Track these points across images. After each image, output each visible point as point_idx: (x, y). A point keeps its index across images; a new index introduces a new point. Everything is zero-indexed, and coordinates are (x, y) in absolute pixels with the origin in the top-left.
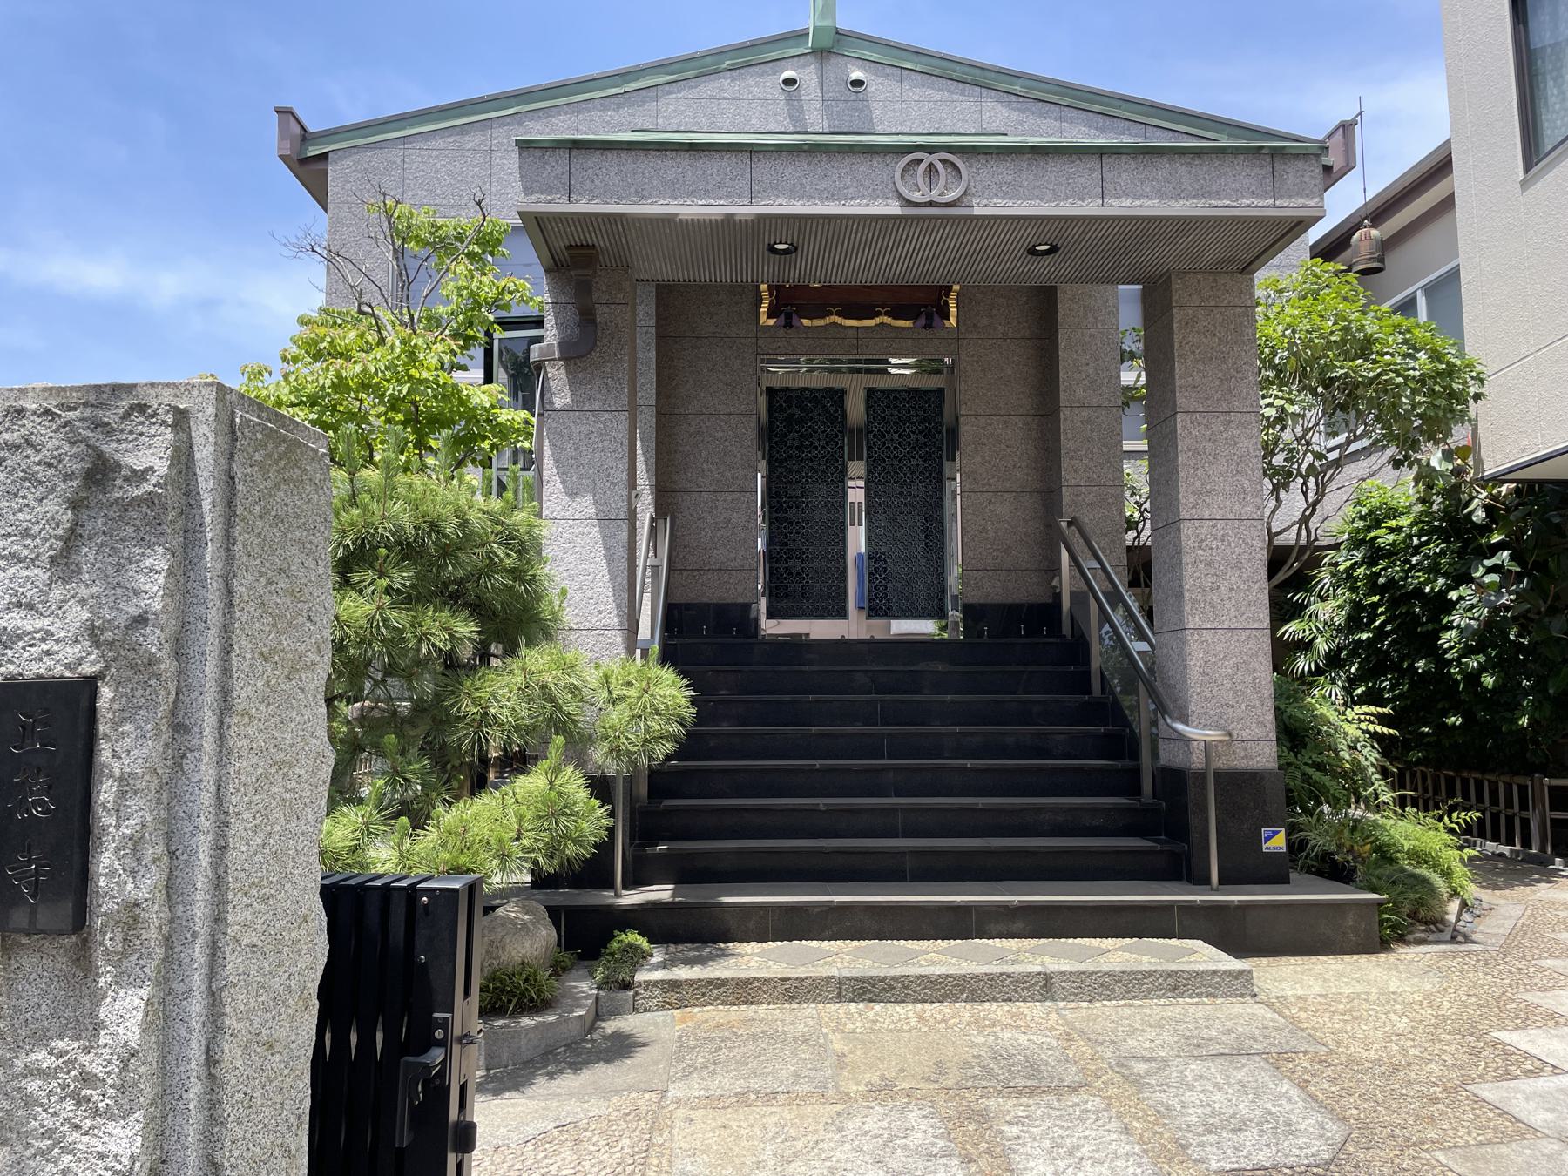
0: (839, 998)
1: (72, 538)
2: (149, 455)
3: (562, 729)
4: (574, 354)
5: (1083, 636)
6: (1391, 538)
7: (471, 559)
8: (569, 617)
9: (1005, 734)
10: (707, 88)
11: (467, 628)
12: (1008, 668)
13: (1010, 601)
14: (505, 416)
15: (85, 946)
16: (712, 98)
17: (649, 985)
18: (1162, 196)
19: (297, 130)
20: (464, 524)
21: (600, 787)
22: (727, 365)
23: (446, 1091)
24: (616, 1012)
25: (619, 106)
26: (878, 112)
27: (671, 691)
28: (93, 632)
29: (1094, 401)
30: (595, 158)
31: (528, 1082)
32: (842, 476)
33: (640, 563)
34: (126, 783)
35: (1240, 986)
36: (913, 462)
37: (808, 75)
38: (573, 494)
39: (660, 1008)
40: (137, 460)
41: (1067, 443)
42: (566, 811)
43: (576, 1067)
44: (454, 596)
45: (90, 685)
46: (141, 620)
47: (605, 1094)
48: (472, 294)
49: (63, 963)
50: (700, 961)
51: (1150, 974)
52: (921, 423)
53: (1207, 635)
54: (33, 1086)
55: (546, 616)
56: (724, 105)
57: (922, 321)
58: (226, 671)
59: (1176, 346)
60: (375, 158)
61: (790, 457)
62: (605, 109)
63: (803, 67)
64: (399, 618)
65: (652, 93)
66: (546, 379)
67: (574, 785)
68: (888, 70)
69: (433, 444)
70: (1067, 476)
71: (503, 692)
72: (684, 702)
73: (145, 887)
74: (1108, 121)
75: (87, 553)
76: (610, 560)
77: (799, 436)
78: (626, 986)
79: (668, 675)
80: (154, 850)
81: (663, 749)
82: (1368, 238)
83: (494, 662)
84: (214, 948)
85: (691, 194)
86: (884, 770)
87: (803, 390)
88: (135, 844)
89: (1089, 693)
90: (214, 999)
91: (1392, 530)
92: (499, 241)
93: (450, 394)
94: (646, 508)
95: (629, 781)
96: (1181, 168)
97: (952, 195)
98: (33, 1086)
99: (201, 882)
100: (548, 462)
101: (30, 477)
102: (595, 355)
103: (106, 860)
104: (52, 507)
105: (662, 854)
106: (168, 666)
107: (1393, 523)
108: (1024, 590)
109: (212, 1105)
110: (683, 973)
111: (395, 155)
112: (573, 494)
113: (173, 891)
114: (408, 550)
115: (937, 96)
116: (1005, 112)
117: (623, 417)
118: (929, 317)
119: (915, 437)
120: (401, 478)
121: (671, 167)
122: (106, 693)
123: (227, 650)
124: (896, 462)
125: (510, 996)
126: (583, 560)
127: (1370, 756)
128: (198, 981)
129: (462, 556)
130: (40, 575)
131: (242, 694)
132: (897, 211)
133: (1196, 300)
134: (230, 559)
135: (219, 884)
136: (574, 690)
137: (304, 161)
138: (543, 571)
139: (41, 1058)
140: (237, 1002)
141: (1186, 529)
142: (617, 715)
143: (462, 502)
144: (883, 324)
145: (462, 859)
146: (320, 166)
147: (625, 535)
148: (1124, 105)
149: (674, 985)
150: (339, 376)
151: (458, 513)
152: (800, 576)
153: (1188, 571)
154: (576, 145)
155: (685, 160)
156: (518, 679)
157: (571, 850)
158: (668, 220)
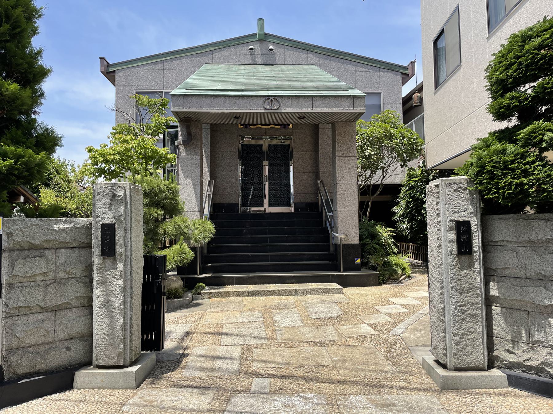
0: (248, 295)
1: (111, 205)
2: (121, 193)
3: (183, 235)
4: (186, 143)
6: (413, 184)
7: (162, 196)
8: (186, 209)
10: (227, 51)
11: (161, 212)
14: (169, 156)
16: (229, 54)
17: (204, 293)
19: (106, 63)
20: (160, 188)
21: (193, 249)
23: (161, 286)
24: (197, 299)
25: (201, 56)
26: (277, 58)
27: (210, 227)
28: (114, 217)
31: (176, 311)
32: (262, 167)
33: (205, 192)
34: (120, 237)
35: (339, 291)
38: (186, 178)
39: (207, 298)
41: (321, 160)
42: (184, 252)
43: (187, 308)
44: (158, 205)
45: (114, 224)
46: (121, 216)
47: (193, 312)
48: (159, 122)
50: (217, 289)
53: (343, 212)
54: (108, 276)
55: (179, 208)
56: (232, 56)
58: (131, 222)
60: (129, 72)
62: (197, 57)
66: (179, 149)
67: (186, 247)
69: (150, 163)
70: (321, 169)
71: (169, 227)
72: (213, 229)
73: (122, 250)
74: (345, 61)
75: (113, 207)
76: (196, 194)
77: (250, 156)
78: (199, 294)
79: (209, 222)
80: (123, 246)
81: (207, 240)
82: (417, 96)
83: (167, 220)
84: (131, 259)
85: (213, 107)
86: (267, 246)
87: (251, 145)
88: (121, 245)
90: (131, 266)
91: (414, 181)
92: (166, 105)
93: (154, 152)
94: (207, 177)
95: (202, 248)
97: (276, 107)
98: (108, 276)
100: (180, 170)
101: (104, 196)
102: (191, 143)
103: (117, 247)
104: (108, 200)
105: (209, 266)
106: (124, 222)
107: (414, 179)
108: (310, 199)
109: (131, 279)
110: (212, 291)
111: (135, 71)
112: (186, 178)
113: (126, 251)
115: (295, 53)
117: (199, 159)
119: (281, 156)
120: (145, 178)
122: (116, 225)
123: (131, 219)
125: (173, 295)
126: (189, 194)
127: (390, 241)
128: (129, 263)
129: (160, 196)
131: (133, 225)
132: (263, 111)
133: (341, 129)
134: (131, 207)
135: (131, 251)
136: (186, 226)
138: (178, 198)
139: (109, 273)
140: (134, 266)
141: (338, 186)
142: (196, 232)
143: (159, 183)
146: (113, 74)
147: (199, 188)
149: (210, 293)
150: (126, 148)
151: (159, 186)
153: (338, 196)
155: (212, 99)
156: (173, 224)
157: (185, 261)
158: (209, 113)
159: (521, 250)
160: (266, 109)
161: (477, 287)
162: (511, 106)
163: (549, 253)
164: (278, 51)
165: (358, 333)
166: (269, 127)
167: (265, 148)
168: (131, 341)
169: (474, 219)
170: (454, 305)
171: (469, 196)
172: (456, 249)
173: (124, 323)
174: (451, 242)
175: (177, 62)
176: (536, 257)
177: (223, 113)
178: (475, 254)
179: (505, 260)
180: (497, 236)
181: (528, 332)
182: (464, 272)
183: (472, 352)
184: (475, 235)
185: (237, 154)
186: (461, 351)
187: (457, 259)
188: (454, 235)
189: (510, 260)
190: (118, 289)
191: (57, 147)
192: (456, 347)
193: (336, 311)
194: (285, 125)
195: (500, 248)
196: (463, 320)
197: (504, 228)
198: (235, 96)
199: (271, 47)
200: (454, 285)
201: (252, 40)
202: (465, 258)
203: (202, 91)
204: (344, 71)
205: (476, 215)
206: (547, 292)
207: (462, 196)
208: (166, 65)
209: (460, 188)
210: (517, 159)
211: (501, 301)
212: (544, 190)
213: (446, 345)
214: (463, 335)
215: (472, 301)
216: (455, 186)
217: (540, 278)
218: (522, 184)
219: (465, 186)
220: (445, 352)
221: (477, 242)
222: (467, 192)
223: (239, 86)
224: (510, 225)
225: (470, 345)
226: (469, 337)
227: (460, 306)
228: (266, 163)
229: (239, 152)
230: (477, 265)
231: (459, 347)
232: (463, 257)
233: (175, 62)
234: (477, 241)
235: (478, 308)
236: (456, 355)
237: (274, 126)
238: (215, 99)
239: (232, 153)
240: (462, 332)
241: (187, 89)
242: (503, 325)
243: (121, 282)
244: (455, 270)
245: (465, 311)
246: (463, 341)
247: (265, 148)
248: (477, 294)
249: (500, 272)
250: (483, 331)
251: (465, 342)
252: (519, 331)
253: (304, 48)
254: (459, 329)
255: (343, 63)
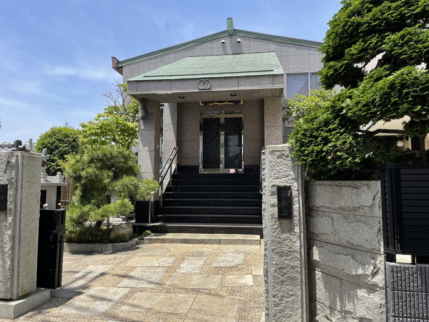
0: (181, 243)
2: (13, 161)
9: (239, 194)
10: (204, 46)
15: (6, 212)
18: (250, 86)
19: (116, 61)
20: (111, 154)
25: (185, 51)
30: (141, 83)
37: (227, 41)
38: (144, 146)
40: (12, 161)
45: (7, 185)
49: (4, 214)
51: (239, 240)
60: (132, 66)
62: (182, 52)
63: (226, 39)
64: (97, 172)
65: (192, 48)
68: (246, 38)
74: (300, 47)
76: (151, 159)
77: (209, 128)
78: (143, 239)
85: (159, 89)
88: (11, 202)
90: (20, 219)
96: (254, 79)
99: (19, 206)
103: (8, 203)
105: (160, 217)
106: (15, 183)
109: (20, 230)
111: (137, 65)
112: (144, 146)
113: (16, 207)
114: (101, 160)
115: (258, 43)
116: (274, 46)
119: (235, 127)
121: (155, 84)
122: (9, 186)
130: (3, 173)
131: (24, 186)
132: (198, 91)
133: (269, 103)
137: (118, 68)
139: (3, 224)
144: (227, 104)
145: (104, 214)
146: (121, 69)
148: (304, 42)
149: (151, 239)
152: (211, 160)
154: (138, 81)
155: (158, 82)
158: (156, 94)
159: (335, 216)
160: (200, 89)
161: (296, 251)
162: (329, 74)
163: (356, 222)
164: (244, 42)
165: (238, 283)
166: (224, 104)
167: (222, 121)
168: (18, 280)
169: (296, 184)
170: (274, 267)
171: (291, 162)
172: (277, 213)
173: (12, 265)
174: (273, 206)
175: (167, 57)
176: (346, 225)
177: (167, 94)
178: (295, 218)
179: (323, 225)
180: (318, 201)
181: (342, 301)
182: (284, 236)
183: (291, 315)
184: (295, 199)
185: (198, 127)
186: (280, 312)
187: (278, 223)
188: (276, 200)
189: (327, 226)
190: (7, 238)
191: (407, 122)
192: (275, 308)
193: (239, 259)
194: (236, 102)
195: (321, 213)
196: (282, 282)
197: (325, 194)
198: (175, 80)
199: (238, 40)
200: (275, 247)
201: (223, 36)
202: (285, 222)
203: (153, 77)
204: (299, 55)
205: (297, 181)
206: (354, 261)
207: (284, 163)
208: (159, 60)
209: (283, 155)
210: (321, 127)
211: (321, 266)
212: (340, 157)
213: (268, 305)
214: (282, 297)
215: (292, 264)
216: (278, 154)
217: (349, 246)
218: (322, 151)
219: (288, 153)
220: (267, 312)
221: (297, 206)
222: (289, 159)
223: (190, 71)
224: (327, 192)
225: (289, 308)
226: (288, 300)
227: (280, 268)
228: (222, 133)
229: (201, 125)
230: (297, 230)
231: (278, 308)
232: (284, 221)
233: (165, 57)
234: (298, 205)
235: (297, 271)
236: (275, 316)
237: (228, 103)
238: (160, 83)
239: (195, 126)
240: (281, 294)
241: (145, 77)
242: (323, 290)
243: (9, 232)
244: (276, 233)
245: (285, 274)
246: (282, 303)
247: (222, 121)
248: (296, 257)
249: (321, 236)
250: (302, 294)
251: (284, 305)
252: (335, 299)
253: (266, 39)
254: (279, 291)
255: (298, 49)
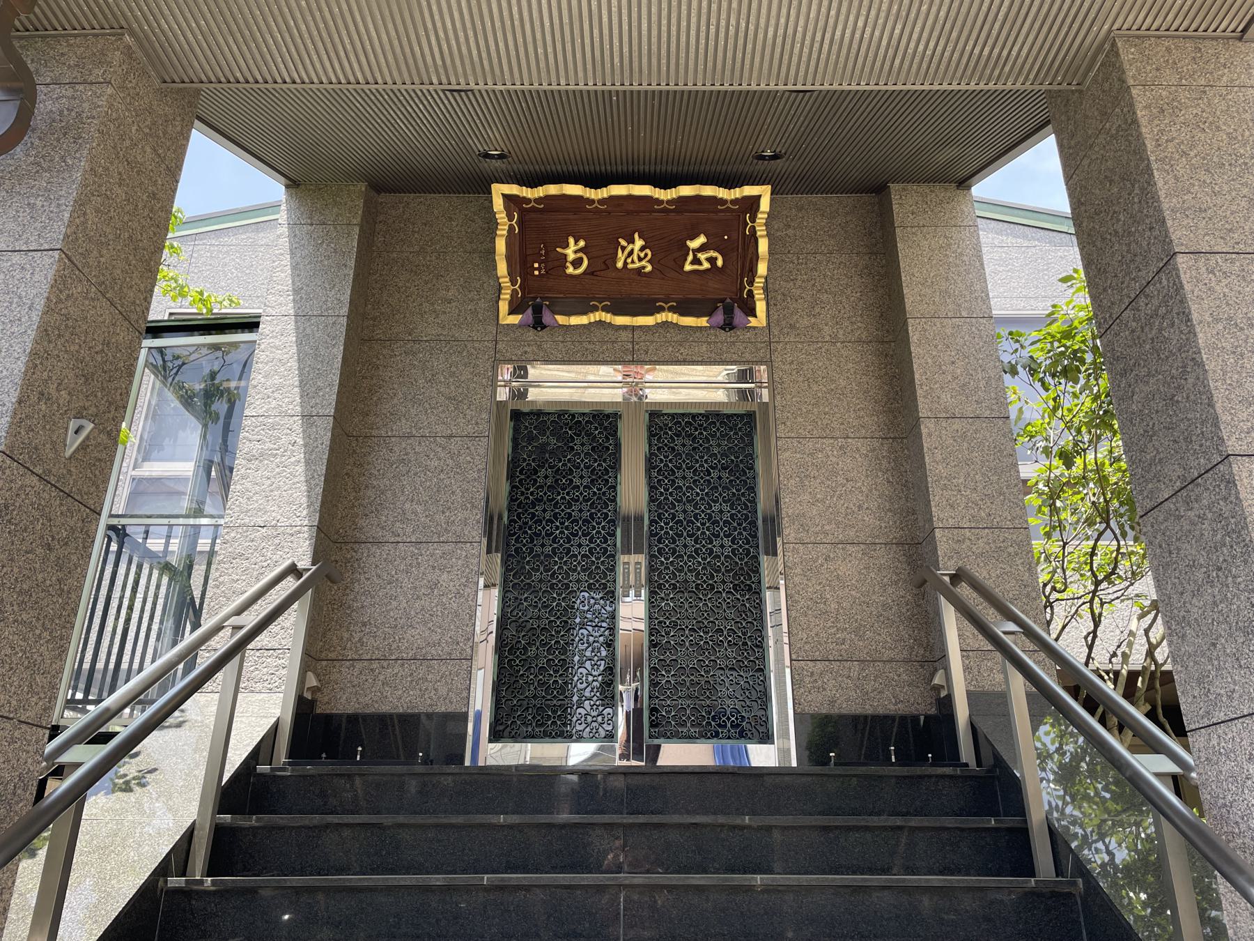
5: (999, 761)
12: (875, 821)
13: (869, 710)
22: (452, 374)
29: (969, 410)
36: (716, 507)
52: (724, 455)
57: (719, 317)
59: (1150, 145)
61: (540, 500)
70: (940, 513)
89: (1031, 873)
108: (891, 695)
118: (729, 312)
124: (689, 508)
133: (1170, 77)
144: (665, 324)
